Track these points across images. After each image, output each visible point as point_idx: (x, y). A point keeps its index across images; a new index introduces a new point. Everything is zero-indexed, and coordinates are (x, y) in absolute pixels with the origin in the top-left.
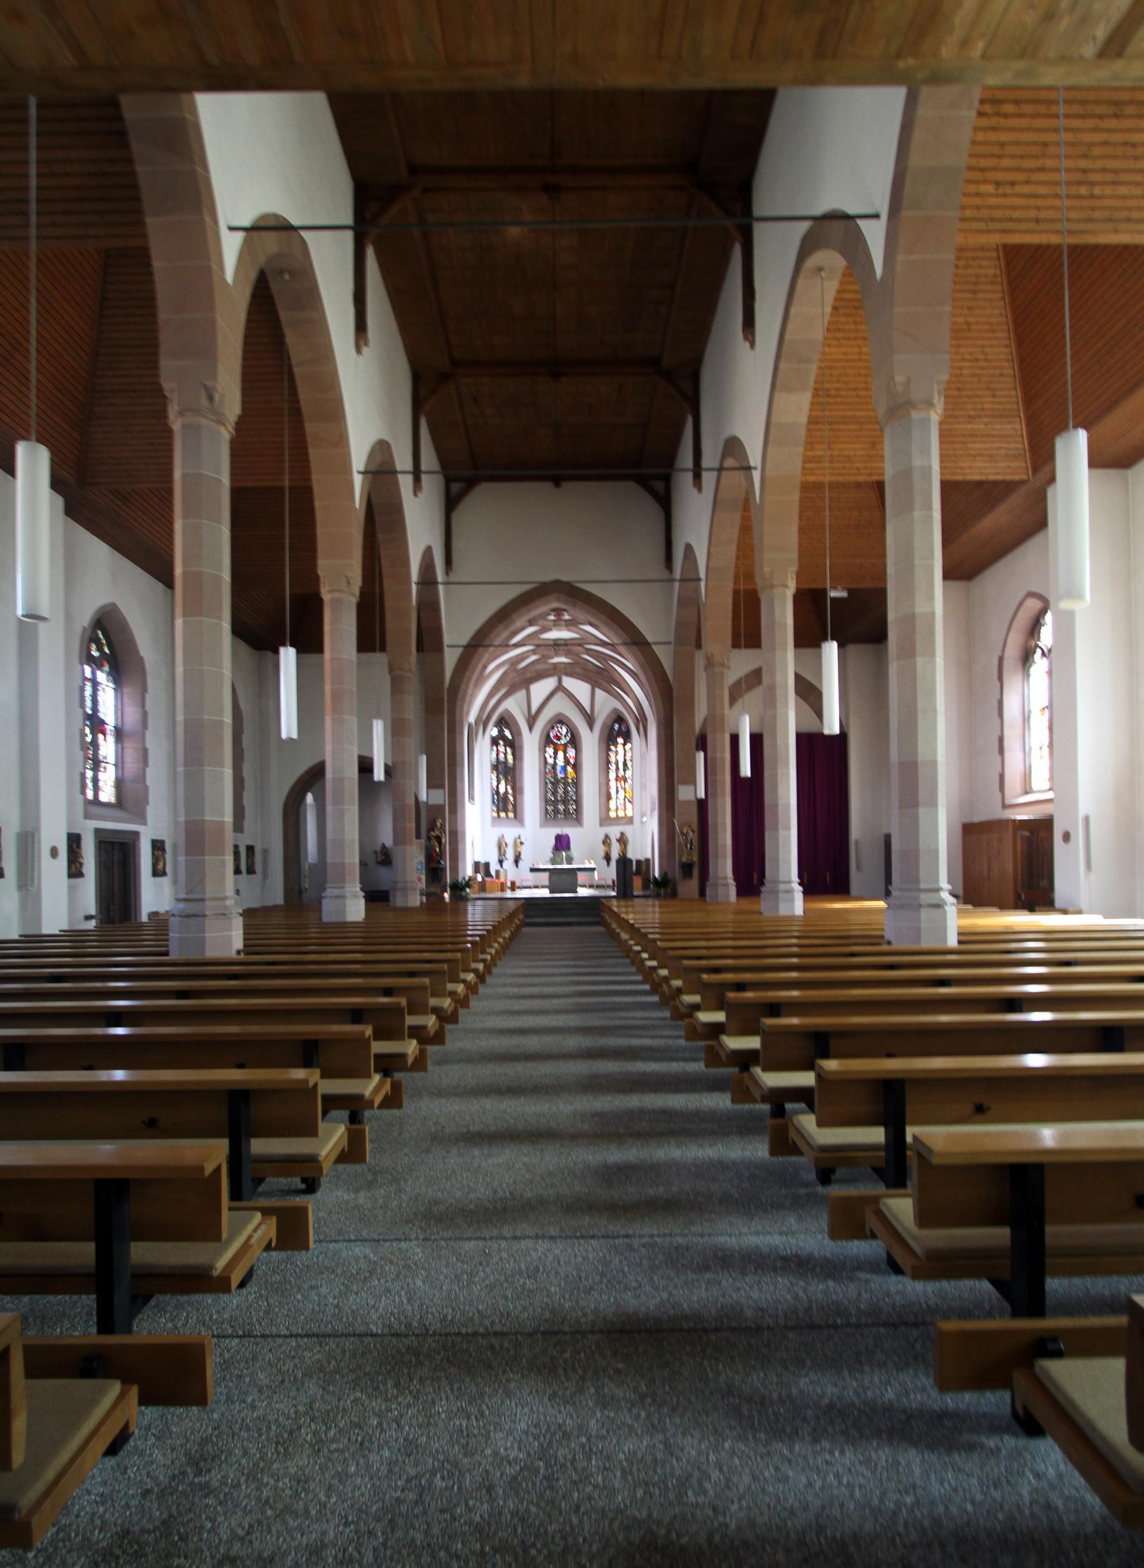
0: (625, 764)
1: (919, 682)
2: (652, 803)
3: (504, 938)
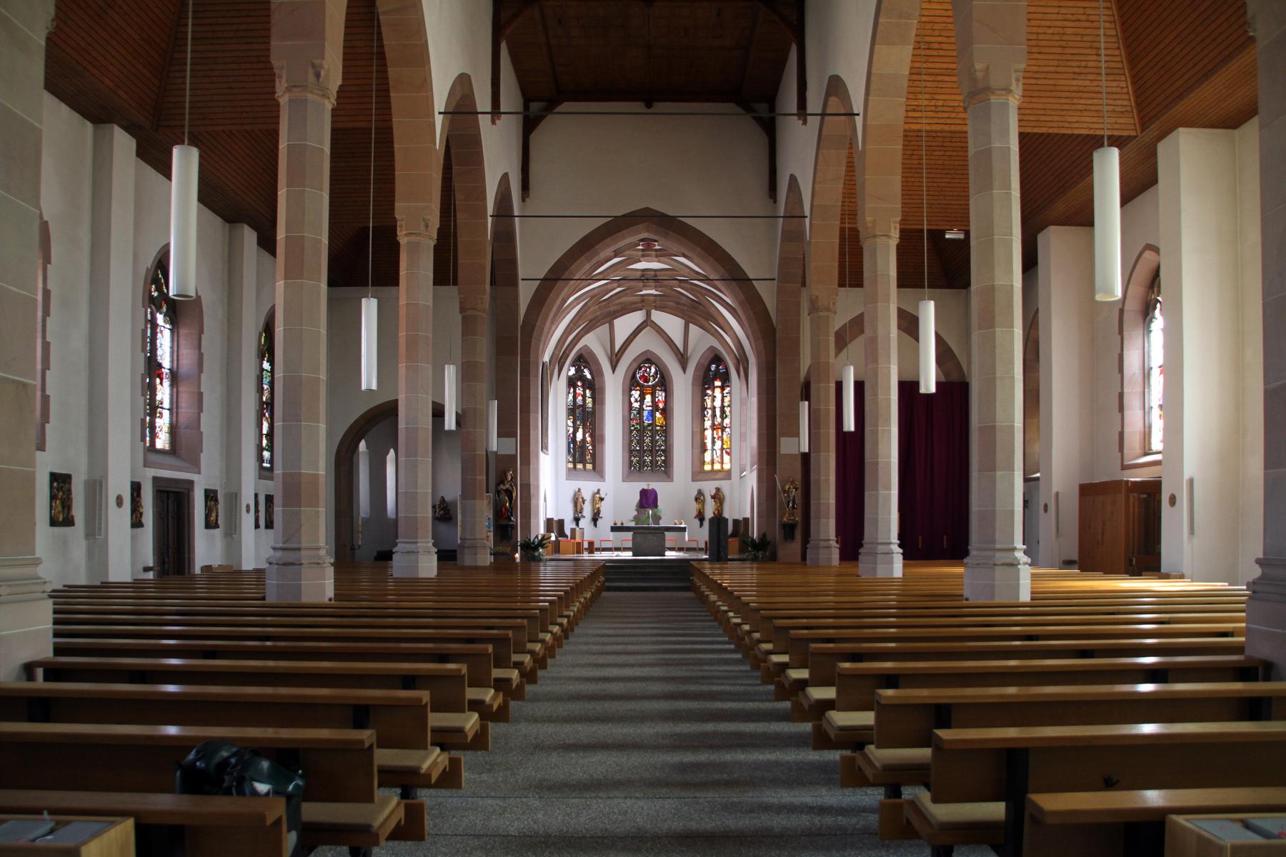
0: (723, 412)
1: (998, 351)
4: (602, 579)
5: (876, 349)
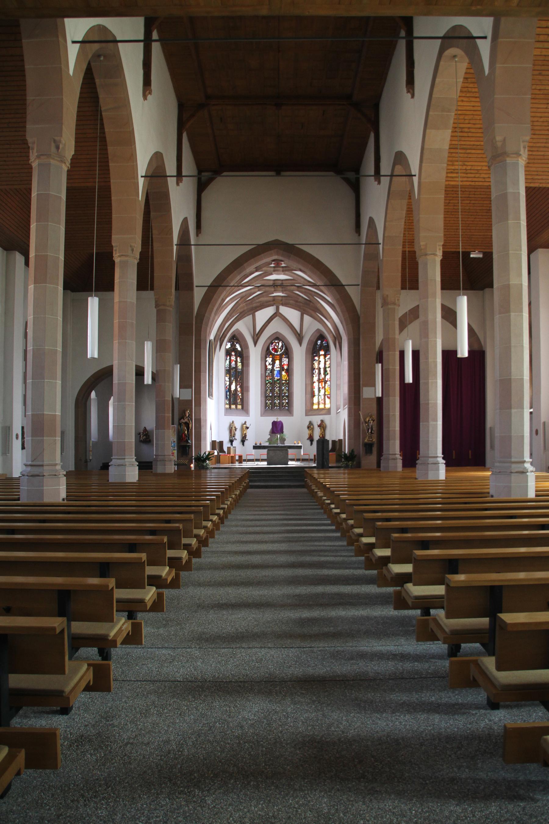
0: (325, 371)
2: (344, 399)
3: (236, 495)
4: (247, 481)
5: (428, 329)
